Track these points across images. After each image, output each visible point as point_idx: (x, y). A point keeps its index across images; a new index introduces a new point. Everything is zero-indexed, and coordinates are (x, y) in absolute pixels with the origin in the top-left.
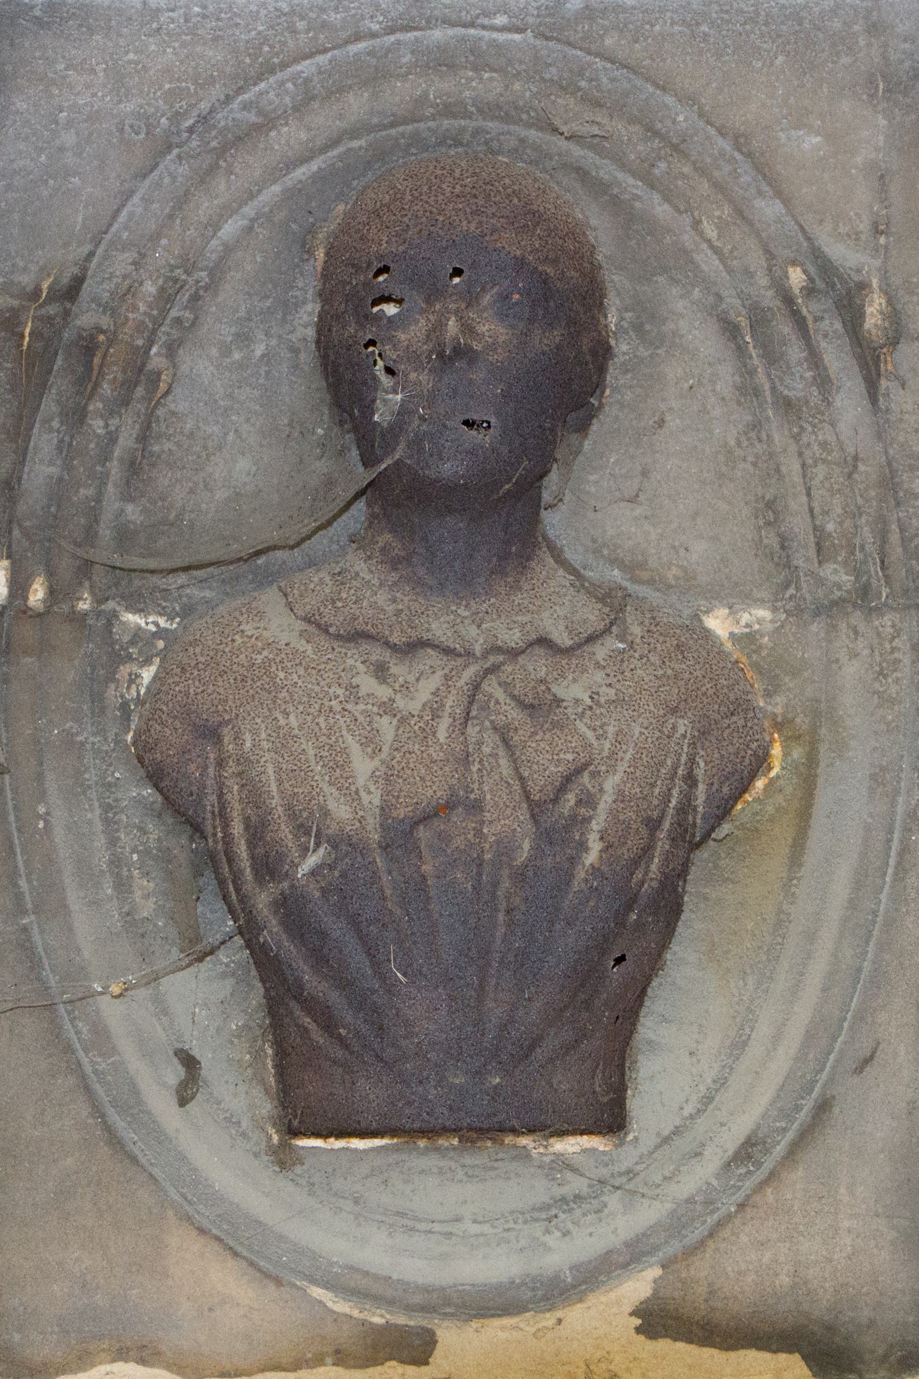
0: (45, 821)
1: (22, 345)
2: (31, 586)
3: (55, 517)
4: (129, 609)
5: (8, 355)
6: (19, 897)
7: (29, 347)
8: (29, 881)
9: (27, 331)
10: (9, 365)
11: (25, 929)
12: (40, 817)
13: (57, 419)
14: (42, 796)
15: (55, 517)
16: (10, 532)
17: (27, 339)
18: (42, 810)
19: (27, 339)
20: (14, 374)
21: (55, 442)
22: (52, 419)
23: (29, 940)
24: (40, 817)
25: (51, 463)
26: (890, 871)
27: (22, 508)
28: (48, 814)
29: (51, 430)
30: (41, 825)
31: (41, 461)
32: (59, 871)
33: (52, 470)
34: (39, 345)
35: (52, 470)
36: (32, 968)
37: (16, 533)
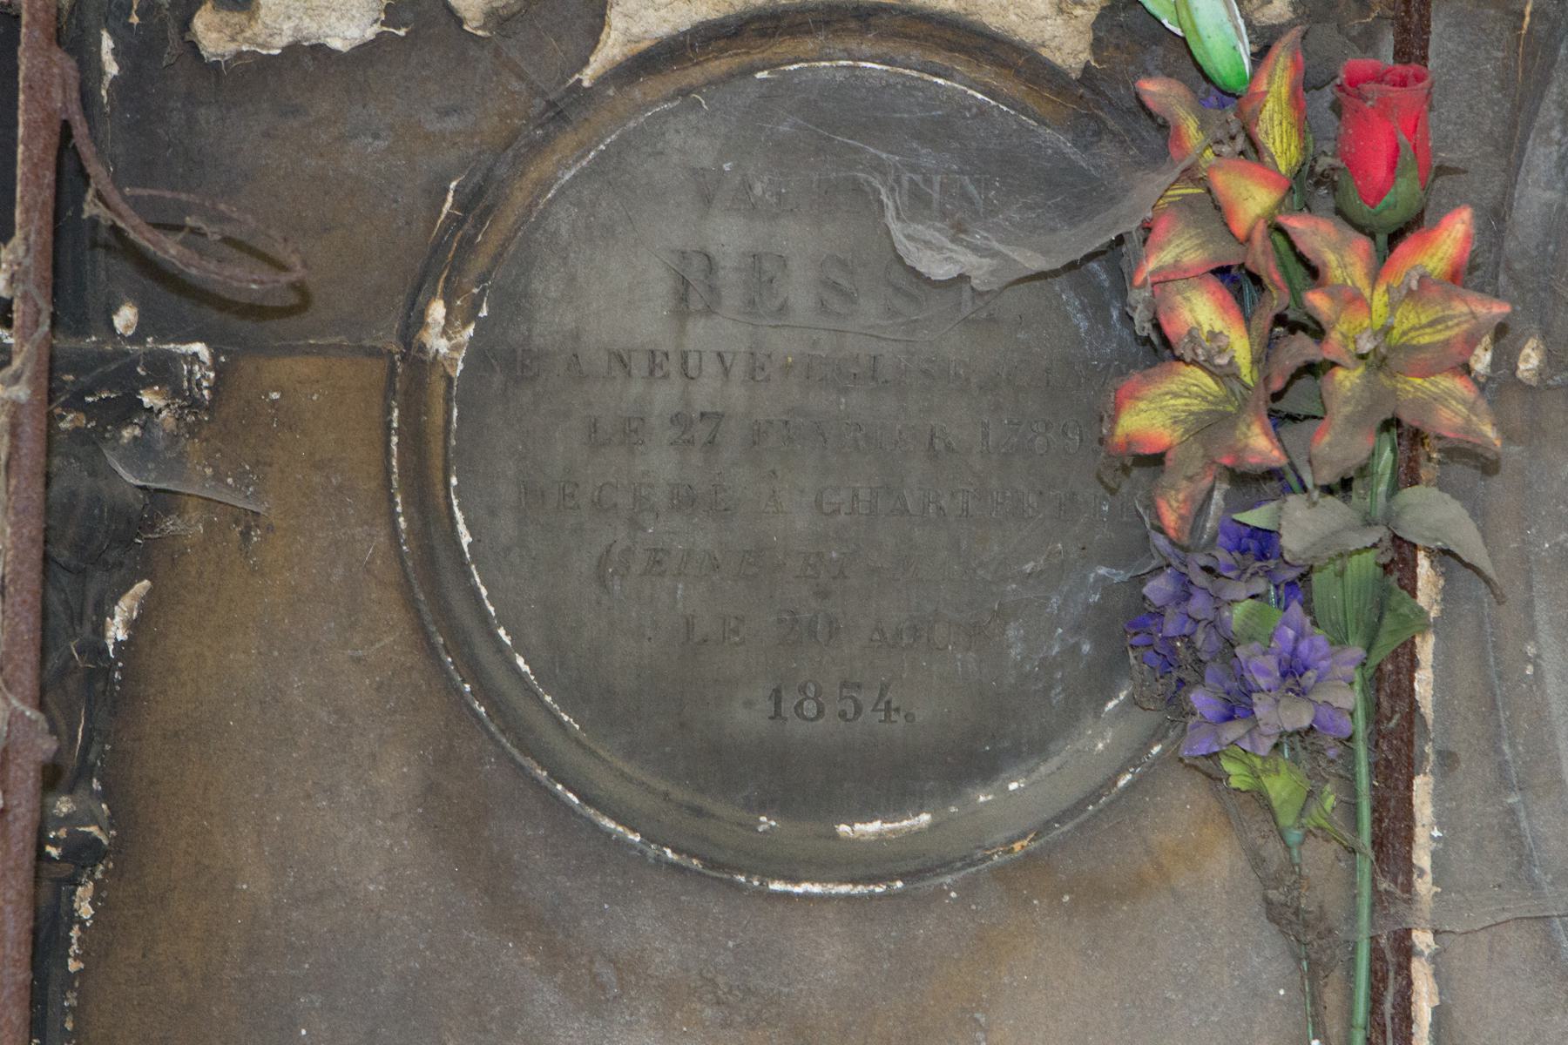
0: (1537, 666)
1: (1521, 28)
2: (1520, 350)
3: (1553, 258)
4: (101, 72)
5: (1499, 40)
6: (1502, 767)
7: (1529, 32)
8: (1513, 745)
9: (1528, 9)
10: (1500, 55)
11: (1511, 811)
12: (1528, 660)
13: (1558, 128)
14: (1531, 633)
15: (1553, 258)
16: (1497, 278)
17: (1527, 19)
18: (1531, 650)
19: (1527, 19)
20: (1506, 67)
21: (1555, 156)
22: (1551, 127)
23: (1516, 825)
24: (1528, 660)
25: (1550, 186)
26: (860, 889)
27: (1510, 245)
28: (1538, 656)
29: (1549, 142)
30: (1529, 670)
31: (1536, 182)
32: (1552, 735)
33: (1549, 195)
34: (1542, 28)
35: (1549, 195)
36: (1519, 865)
37: (1502, 278)
